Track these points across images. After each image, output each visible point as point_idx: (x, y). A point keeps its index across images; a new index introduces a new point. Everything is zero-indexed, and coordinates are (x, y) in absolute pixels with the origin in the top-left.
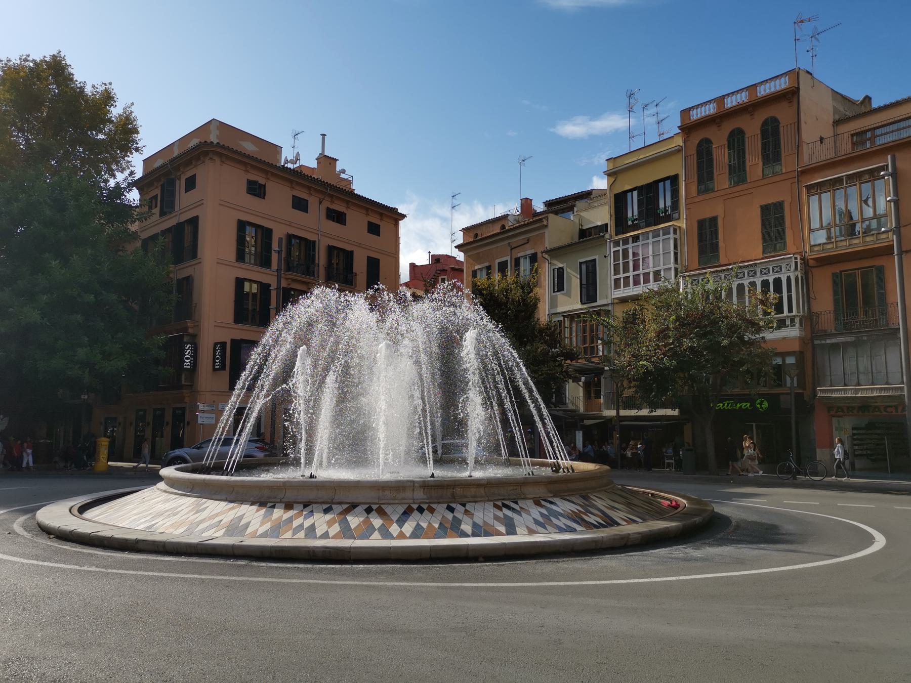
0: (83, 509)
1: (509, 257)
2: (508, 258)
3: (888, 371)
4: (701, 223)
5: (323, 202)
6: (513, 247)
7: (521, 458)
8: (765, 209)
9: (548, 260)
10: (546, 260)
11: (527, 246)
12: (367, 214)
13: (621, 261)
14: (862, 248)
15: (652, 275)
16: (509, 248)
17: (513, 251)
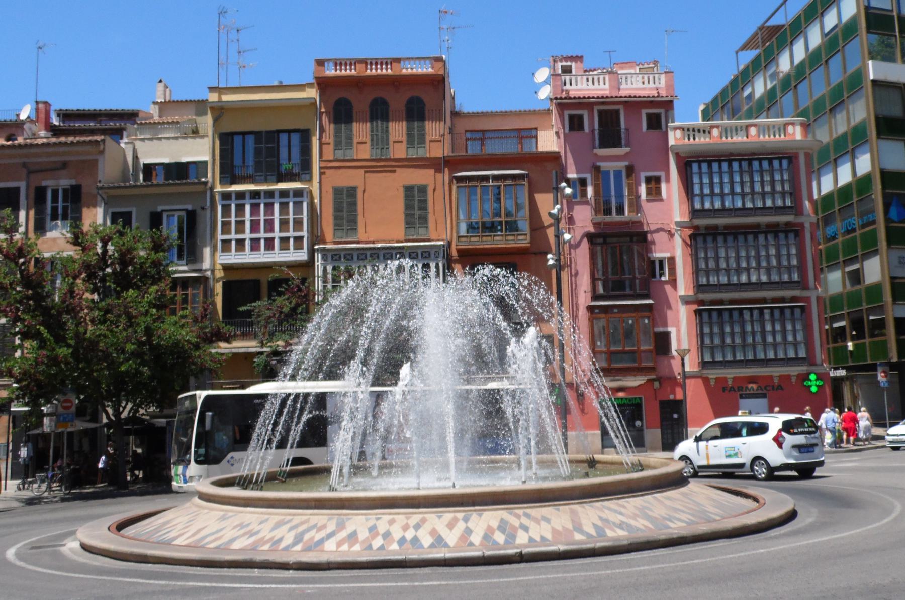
0: (121, 526)
2: (22, 185)
4: (338, 192)
7: (557, 455)
8: (409, 190)
11: (64, 172)
13: (233, 219)
14: (504, 246)
15: (247, 243)
16: (24, 171)
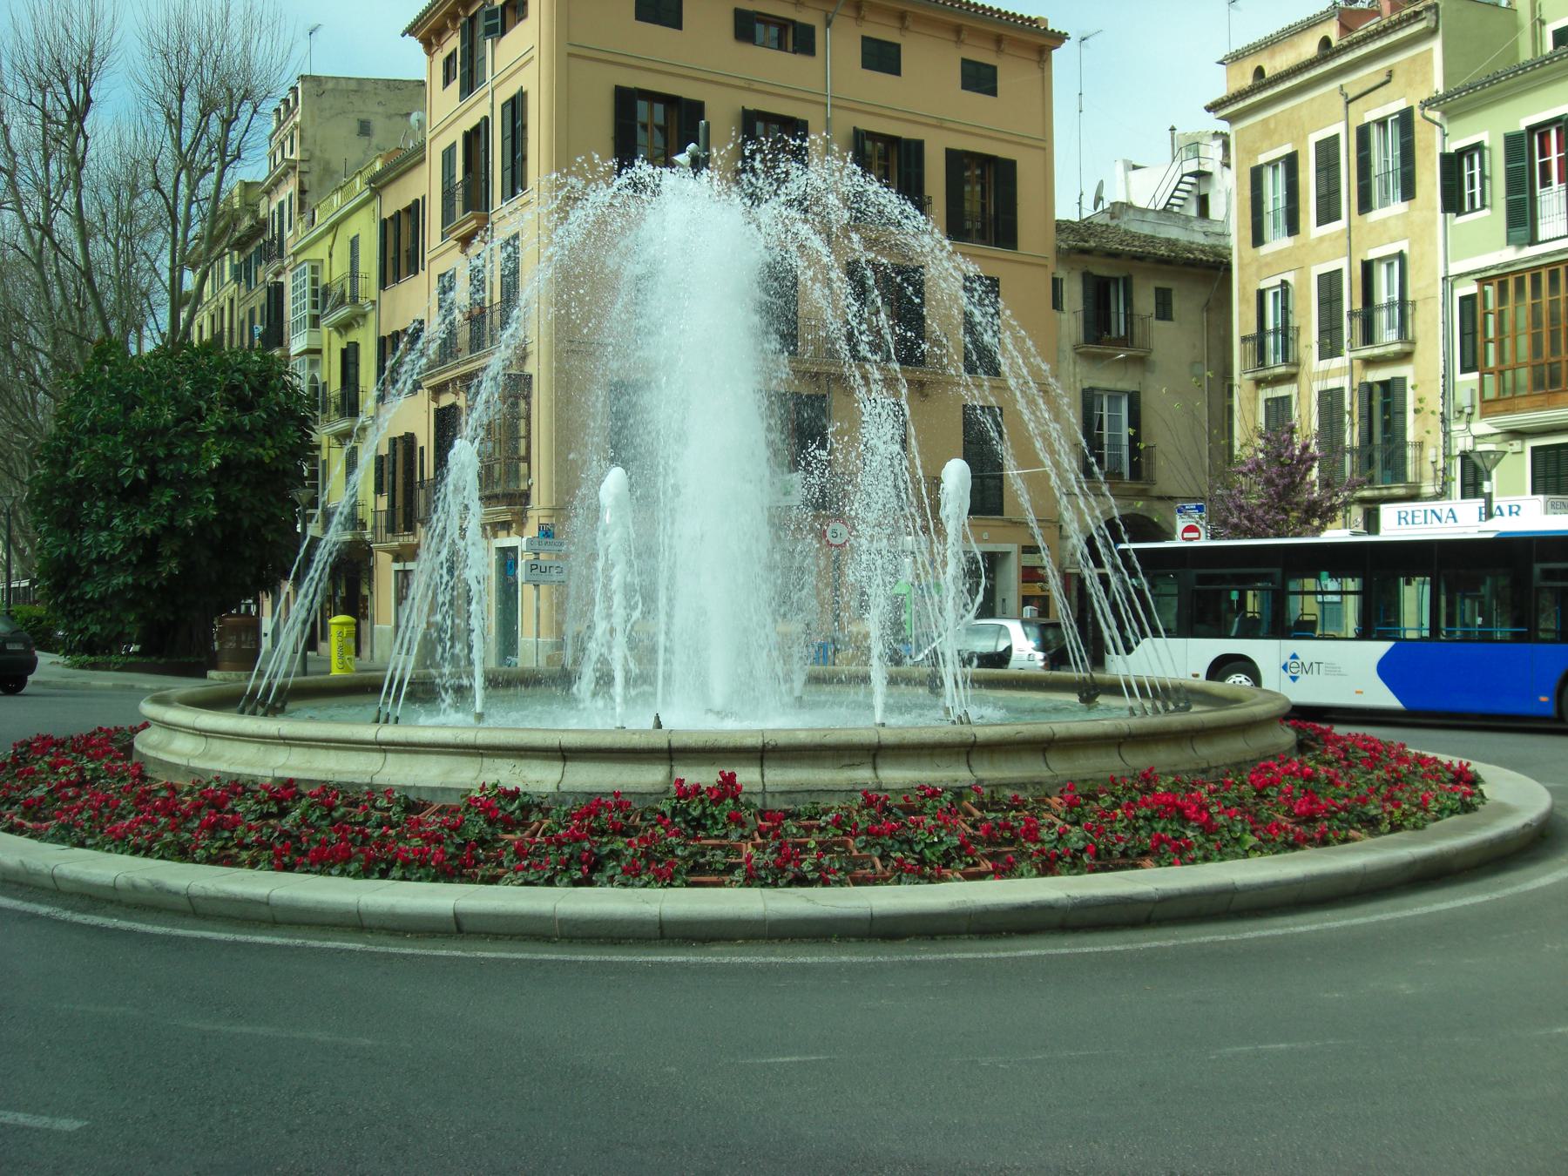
1: (1343, 124)
3: (1410, 297)
5: (834, 21)
6: (1350, 97)
9: (1441, 126)
10: (1437, 127)
12: (959, 41)
16: (1342, 101)
17: (1351, 106)
